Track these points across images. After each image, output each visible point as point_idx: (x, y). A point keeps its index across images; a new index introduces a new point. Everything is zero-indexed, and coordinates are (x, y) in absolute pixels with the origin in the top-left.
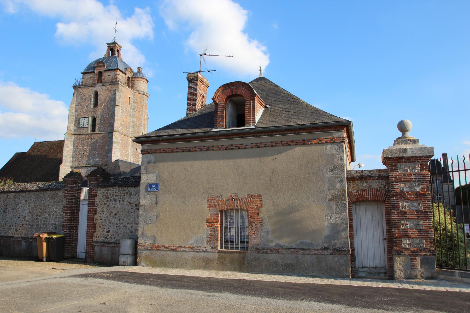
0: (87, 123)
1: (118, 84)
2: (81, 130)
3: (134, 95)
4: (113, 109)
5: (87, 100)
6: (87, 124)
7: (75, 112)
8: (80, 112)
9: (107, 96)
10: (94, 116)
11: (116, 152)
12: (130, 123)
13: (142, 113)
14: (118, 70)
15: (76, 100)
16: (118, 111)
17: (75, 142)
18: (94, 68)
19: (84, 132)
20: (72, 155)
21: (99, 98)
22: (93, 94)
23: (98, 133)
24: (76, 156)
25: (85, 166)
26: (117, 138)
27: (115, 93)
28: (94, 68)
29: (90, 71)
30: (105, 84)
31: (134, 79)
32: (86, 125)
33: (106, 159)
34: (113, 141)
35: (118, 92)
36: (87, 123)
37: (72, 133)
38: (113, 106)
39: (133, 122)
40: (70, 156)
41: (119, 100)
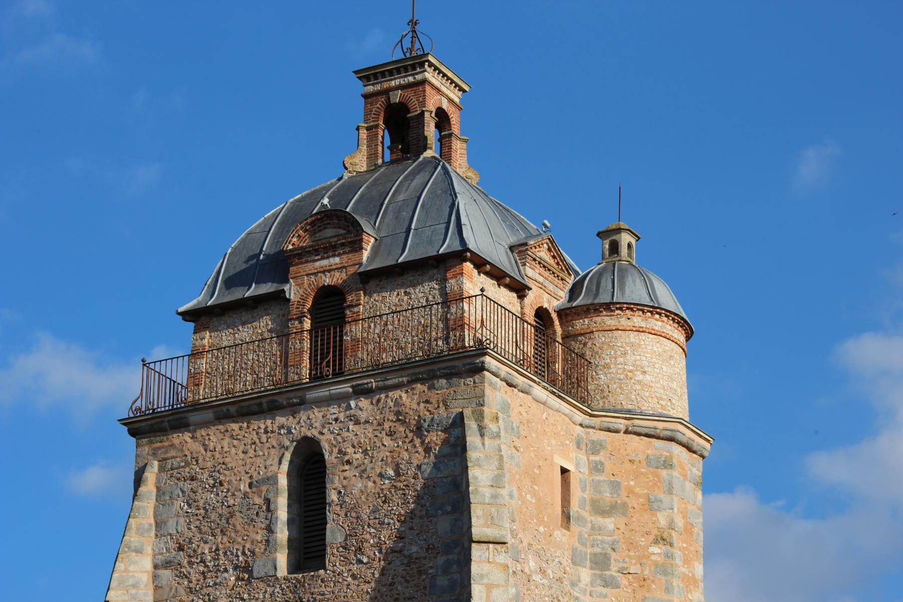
1: (482, 368)
3: (595, 448)
5: (238, 520)
9: (398, 473)
13: (668, 589)
14: (468, 266)
15: (159, 525)
16: (489, 587)
21: (333, 496)
22: (285, 466)
29: (253, 291)
31: (580, 324)
41: (495, 497)
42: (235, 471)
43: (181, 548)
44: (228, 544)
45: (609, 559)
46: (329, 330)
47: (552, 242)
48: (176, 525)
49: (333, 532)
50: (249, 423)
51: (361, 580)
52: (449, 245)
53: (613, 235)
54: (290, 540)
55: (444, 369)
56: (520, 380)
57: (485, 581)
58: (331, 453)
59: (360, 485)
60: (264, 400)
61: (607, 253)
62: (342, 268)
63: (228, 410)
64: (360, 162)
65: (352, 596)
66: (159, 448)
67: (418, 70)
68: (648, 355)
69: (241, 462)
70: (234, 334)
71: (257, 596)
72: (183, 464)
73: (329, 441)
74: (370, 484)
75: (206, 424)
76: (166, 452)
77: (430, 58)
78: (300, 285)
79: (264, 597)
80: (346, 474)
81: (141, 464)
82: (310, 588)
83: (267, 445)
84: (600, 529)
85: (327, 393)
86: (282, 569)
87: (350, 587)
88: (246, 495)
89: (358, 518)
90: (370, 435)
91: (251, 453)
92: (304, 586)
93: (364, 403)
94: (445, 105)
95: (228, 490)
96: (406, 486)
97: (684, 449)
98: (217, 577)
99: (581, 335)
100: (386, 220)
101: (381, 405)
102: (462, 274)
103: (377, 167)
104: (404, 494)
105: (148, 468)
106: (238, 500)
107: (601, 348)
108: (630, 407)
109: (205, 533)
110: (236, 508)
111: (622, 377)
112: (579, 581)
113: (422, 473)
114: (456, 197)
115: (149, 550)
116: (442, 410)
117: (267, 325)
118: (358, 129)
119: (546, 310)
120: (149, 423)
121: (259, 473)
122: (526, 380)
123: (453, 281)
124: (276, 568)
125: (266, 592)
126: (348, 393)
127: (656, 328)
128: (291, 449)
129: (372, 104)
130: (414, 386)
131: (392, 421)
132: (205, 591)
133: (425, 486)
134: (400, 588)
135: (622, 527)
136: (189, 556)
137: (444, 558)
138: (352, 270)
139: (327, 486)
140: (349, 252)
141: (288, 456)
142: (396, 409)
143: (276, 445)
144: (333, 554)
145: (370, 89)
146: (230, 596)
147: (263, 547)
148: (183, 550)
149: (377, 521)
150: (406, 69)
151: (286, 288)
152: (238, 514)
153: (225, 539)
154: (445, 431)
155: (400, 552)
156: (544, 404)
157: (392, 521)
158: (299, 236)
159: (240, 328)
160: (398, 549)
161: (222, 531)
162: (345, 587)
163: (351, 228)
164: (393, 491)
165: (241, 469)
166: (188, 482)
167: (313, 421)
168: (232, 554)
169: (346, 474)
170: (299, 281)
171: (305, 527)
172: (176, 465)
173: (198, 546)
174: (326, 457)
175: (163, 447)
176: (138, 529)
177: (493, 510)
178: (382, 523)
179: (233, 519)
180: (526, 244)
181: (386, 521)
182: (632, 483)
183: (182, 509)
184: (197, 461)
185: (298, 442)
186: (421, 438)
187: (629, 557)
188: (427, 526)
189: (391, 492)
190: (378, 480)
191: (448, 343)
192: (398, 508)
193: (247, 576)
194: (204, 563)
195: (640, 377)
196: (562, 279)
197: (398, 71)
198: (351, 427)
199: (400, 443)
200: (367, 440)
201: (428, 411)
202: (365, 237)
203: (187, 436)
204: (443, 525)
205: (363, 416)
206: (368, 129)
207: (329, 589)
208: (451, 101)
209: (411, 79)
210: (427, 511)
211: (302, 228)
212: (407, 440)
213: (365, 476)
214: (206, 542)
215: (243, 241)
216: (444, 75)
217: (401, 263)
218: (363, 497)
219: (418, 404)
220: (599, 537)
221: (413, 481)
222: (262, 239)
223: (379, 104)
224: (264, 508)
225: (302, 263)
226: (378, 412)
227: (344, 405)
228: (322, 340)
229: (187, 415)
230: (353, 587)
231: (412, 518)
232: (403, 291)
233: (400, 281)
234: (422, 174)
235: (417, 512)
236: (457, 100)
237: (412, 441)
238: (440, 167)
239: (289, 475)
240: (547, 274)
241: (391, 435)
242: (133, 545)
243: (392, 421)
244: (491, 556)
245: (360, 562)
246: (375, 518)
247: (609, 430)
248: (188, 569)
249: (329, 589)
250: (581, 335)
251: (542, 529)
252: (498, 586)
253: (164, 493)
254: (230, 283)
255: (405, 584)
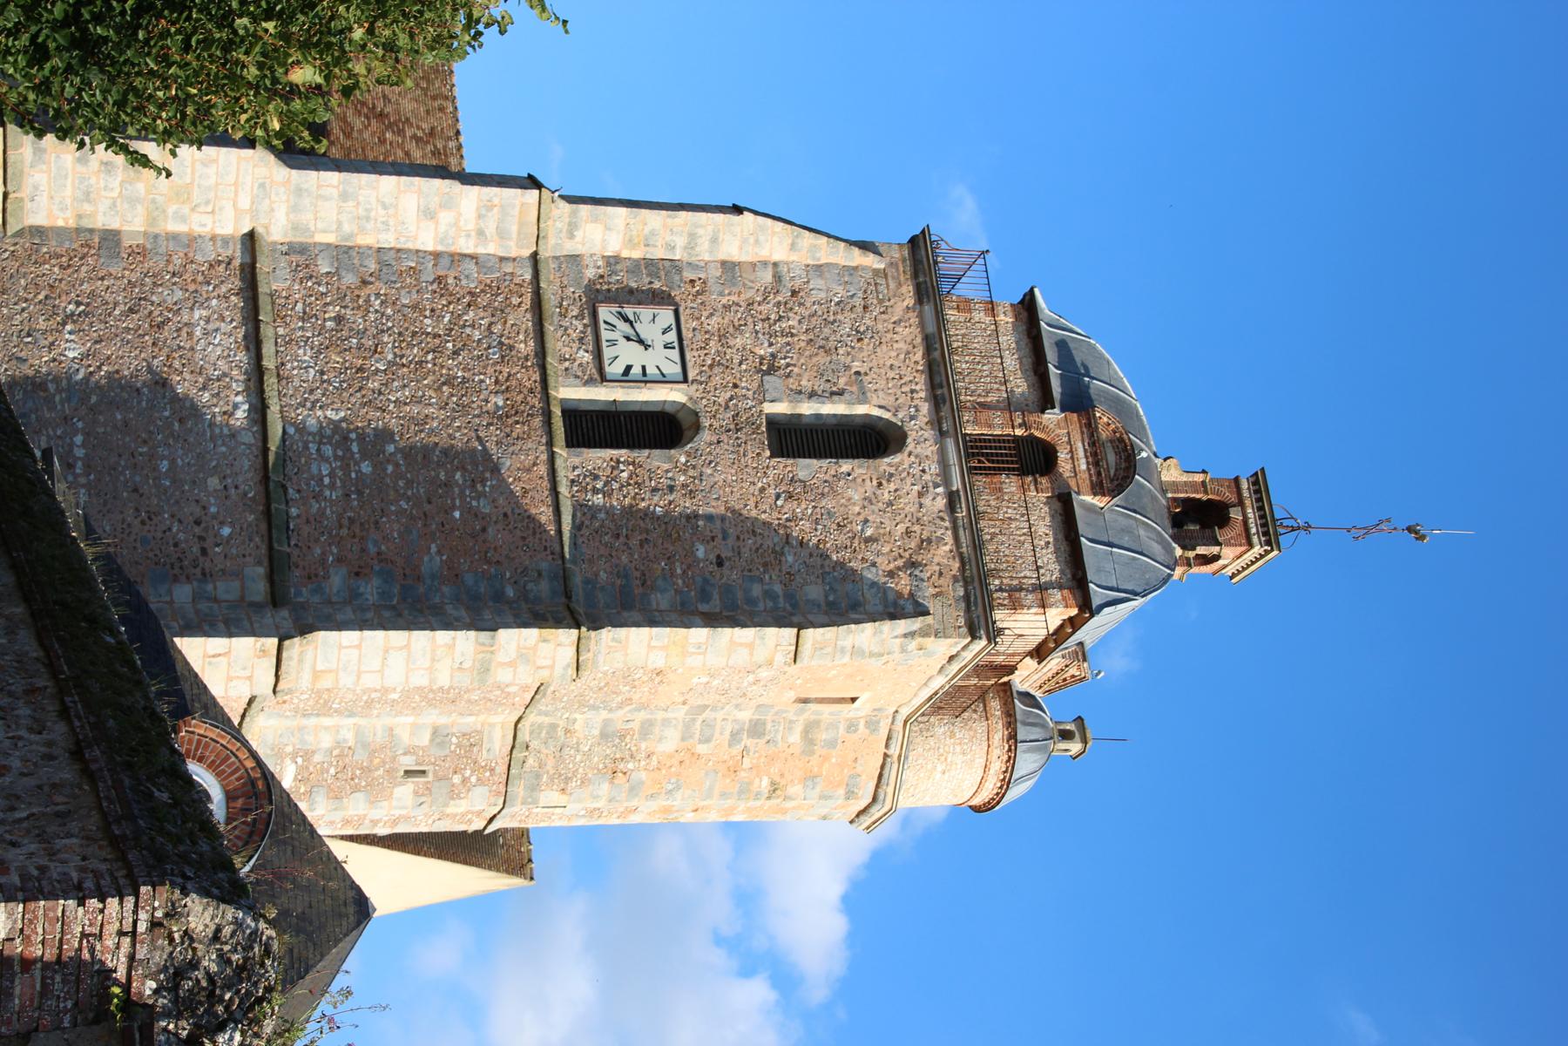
0: (636, 370)
1: (974, 636)
2: (580, 317)
3: (872, 725)
4: (769, 594)
5: (822, 359)
6: (629, 368)
7: (723, 263)
8: (727, 308)
9: (868, 540)
10: (697, 428)
11: (397, 661)
12: (643, 707)
13: (723, 795)
14: (1074, 612)
15: (819, 269)
16: (751, 646)
17: (470, 267)
18: (1079, 403)
19: (557, 344)
20: (362, 240)
21: (846, 466)
22: (876, 412)
23: (564, 476)
24: (349, 279)
25: (269, 363)
26: (524, 656)
27: (894, 615)
28: (1079, 403)
29: (1053, 371)
30: (962, 514)
31: (995, 705)
32: (623, 354)
33: (339, 560)
34: (503, 634)
35: (910, 635)
36: (636, 370)
37: (552, 241)
38: (790, 597)
39: (646, 729)
40: (347, 228)
41: (843, 650)
42: (873, 356)
43: (794, 293)
44: (798, 347)
45: (759, 738)
46: (1017, 463)
47: (1081, 680)
48: (819, 289)
49: (808, 466)
50: (922, 372)
51: (759, 498)
52: (1098, 594)
53: (1080, 734)
54: (800, 415)
55: (975, 595)
56: (955, 667)
57: (758, 642)
58: (890, 465)
59: (856, 498)
60: (945, 390)
61: (1062, 727)
62: (1075, 472)
63: (936, 349)
64: (1171, 473)
65: (742, 487)
66: (897, 270)
67: (1263, 539)
68: (960, 776)
69: (881, 362)
70: (1008, 349)
71: (744, 379)
72: (881, 297)
73: (901, 463)
74: (857, 509)
75: (922, 325)
76: (893, 278)
77: (1275, 552)
78: (1058, 425)
79: (743, 388)
80: (868, 481)
81: (881, 249)
82: (751, 440)
83: (899, 393)
84: (790, 729)
85: (951, 462)
86: (770, 408)
87: (752, 486)
88: (847, 368)
89: (823, 494)
90: (907, 508)
91: (891, 374)
92: (753, 433)
93: (941, 502)
94: (1221, 562)
95: (853, 348)
96: (855, 551)
97: (862, 808)
98: (764, 334)
99: (985, 706)
100: (1120, 519)
101: (938, 521)
102: (1067, 607)
103: (1164, 492)
104: (846, 547)
105: (877, 258)
106: (842, 359)
107: (970, 729)
108: (910, 758)
109: (809, 321)
110: (835, 357)
111: (941, 750)
112: (740, 710)
113: (868, 568)
114: (1143, 597)
115: (794, 257)
116: (932, 591)
117: (1018, 387)
118: (1204, 472)
119: (1012, 673)
120: (925, 259)
121: (870, 383)
122: (954, 672)
123: (1059, 596)
124: (772, 401)
125: (748, 390)
126: (952, 485)
127: (987, 784)
128: (894, 420)
129: (1229, 487)
130: (957, 559)
131: (921, 534)
132: (750, 320)
133: (854, 571)
134: (750, 541)
135: (791, 750)
136: (786, 303)
137: (780, 593)
138: (1072, 483)
139: (856, 461)
140: (1091, 481)
141: (886, 415)
142: (934, 538)
143: (899, 402)
144: (785, 467)
145: (1244, 485)
146: (744, 349)
147: (794, 387)
148: (792, 296)
149: (819, 516)
150: (1265, 525)
151: (1057, 410)
152: (829, 358)
153: (803, 344)
154: (911, 594)
155: (787, 543)
156: (925, 684)
157: (818, 533)
158: (1109, 424)
159: (1016, 356)
160: (790, 540)
161: (811, 340)
162: (751, 480)
163: (1116, 483)
164: (850, 535)
165: (874, 363)
166: (862, 303)
167: (923, 445)
168: (788, 352)
169: (868, 481)
170: (1063, 424)
171: (806, 430)
172: (881, 288)
173: (796, 313)
174: (886, 460)
175: (899, 274)
176: (815, 246)
177: (829, 650)
178: (817, 522)
179: (823, 354)
180: (1085, 660)
181: (820, 527)
182: (834, 760)
183: (834, 295)
184: (883, 313)
185: (901, 428)
186: (904, 566)
187: (760, 757)
188: (813, 573)
189: (848, 532)
190: (861, 518)
191: (996, 591)
192: (833, 541)
193: (764, 368)
194: (779, 320)
195: (940, 768)
196: (1041, 687)
197: (1263, 517)
198: (916, 487)
199: (899, 543)
200: (902, 505)
201: (932, 575)
202: (1107, 499)
203: (910, 301)
204: (814, 592)
205: (927, 501)
206: (1203, 483)
207: (749, 462)
208: (1225, 567)
209: (1254, 530)
210: (829, 573)
211: (1116, 427)
212: (901, 551)
213: (866, 503)
214: (800, 322)
215: (1101, 356)
216: (1253, 563)
217: (1080, 541)
218: (843, 501)
219: (938, 564)
220: (781, 728)
221: (860, 557)
222: (1102, 378)
223: (1229, 496)
224: (834, 389)
225: (1081, 427)
226: (930, 519)
227: (938, 480)
228: (1006, 455)
229: (932, 303)
230: (752, 489)
231: (821, 556)
232: (1051, 540)
233: (1060, 536)
234: (1162, 551)
235: (827, 562)
236: (1223, 571)
237: (901, 557)
238: (1169, 571)
239: (867, 415)
240: (1050, 675)
241: (907, 533)
242: (799, 241)
243: (921, 534)
244: (783, 648)
245: (778, 497)
246: (822, 515)
247: (889, 738)
248: (773, 302)
249: (749, 462)
250: (985, 706)
251: (799, 682)
252: (751, 655)
253: (851, 275)
254: (1062, 345)
255: (754, 548)
